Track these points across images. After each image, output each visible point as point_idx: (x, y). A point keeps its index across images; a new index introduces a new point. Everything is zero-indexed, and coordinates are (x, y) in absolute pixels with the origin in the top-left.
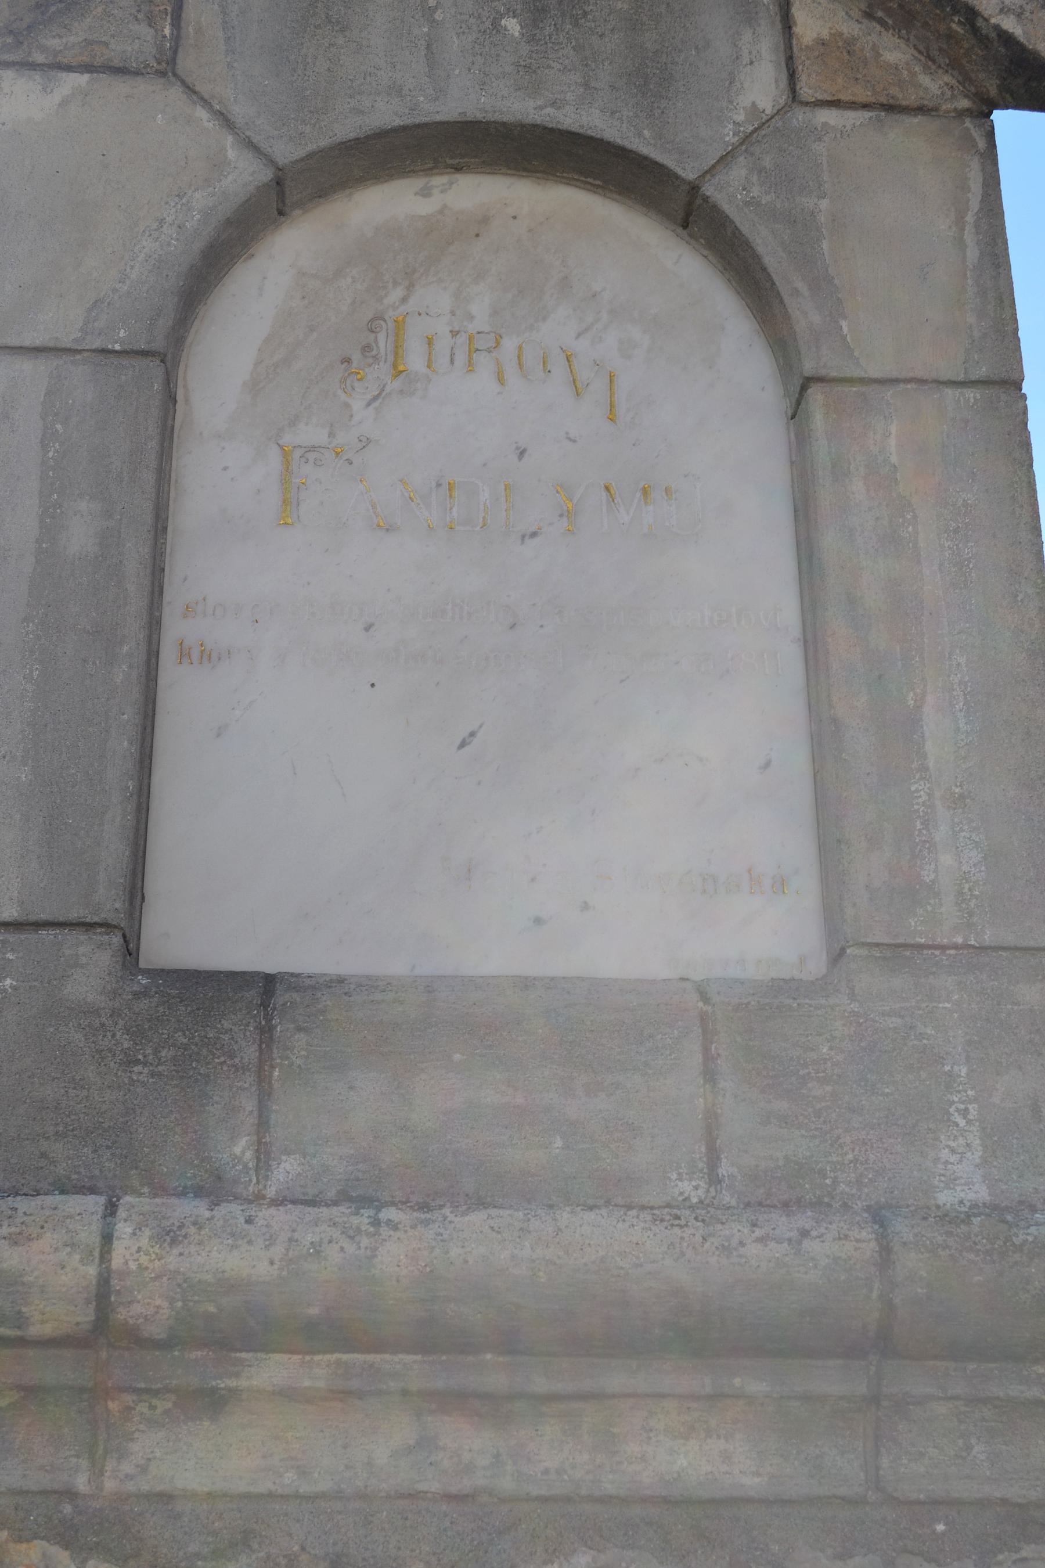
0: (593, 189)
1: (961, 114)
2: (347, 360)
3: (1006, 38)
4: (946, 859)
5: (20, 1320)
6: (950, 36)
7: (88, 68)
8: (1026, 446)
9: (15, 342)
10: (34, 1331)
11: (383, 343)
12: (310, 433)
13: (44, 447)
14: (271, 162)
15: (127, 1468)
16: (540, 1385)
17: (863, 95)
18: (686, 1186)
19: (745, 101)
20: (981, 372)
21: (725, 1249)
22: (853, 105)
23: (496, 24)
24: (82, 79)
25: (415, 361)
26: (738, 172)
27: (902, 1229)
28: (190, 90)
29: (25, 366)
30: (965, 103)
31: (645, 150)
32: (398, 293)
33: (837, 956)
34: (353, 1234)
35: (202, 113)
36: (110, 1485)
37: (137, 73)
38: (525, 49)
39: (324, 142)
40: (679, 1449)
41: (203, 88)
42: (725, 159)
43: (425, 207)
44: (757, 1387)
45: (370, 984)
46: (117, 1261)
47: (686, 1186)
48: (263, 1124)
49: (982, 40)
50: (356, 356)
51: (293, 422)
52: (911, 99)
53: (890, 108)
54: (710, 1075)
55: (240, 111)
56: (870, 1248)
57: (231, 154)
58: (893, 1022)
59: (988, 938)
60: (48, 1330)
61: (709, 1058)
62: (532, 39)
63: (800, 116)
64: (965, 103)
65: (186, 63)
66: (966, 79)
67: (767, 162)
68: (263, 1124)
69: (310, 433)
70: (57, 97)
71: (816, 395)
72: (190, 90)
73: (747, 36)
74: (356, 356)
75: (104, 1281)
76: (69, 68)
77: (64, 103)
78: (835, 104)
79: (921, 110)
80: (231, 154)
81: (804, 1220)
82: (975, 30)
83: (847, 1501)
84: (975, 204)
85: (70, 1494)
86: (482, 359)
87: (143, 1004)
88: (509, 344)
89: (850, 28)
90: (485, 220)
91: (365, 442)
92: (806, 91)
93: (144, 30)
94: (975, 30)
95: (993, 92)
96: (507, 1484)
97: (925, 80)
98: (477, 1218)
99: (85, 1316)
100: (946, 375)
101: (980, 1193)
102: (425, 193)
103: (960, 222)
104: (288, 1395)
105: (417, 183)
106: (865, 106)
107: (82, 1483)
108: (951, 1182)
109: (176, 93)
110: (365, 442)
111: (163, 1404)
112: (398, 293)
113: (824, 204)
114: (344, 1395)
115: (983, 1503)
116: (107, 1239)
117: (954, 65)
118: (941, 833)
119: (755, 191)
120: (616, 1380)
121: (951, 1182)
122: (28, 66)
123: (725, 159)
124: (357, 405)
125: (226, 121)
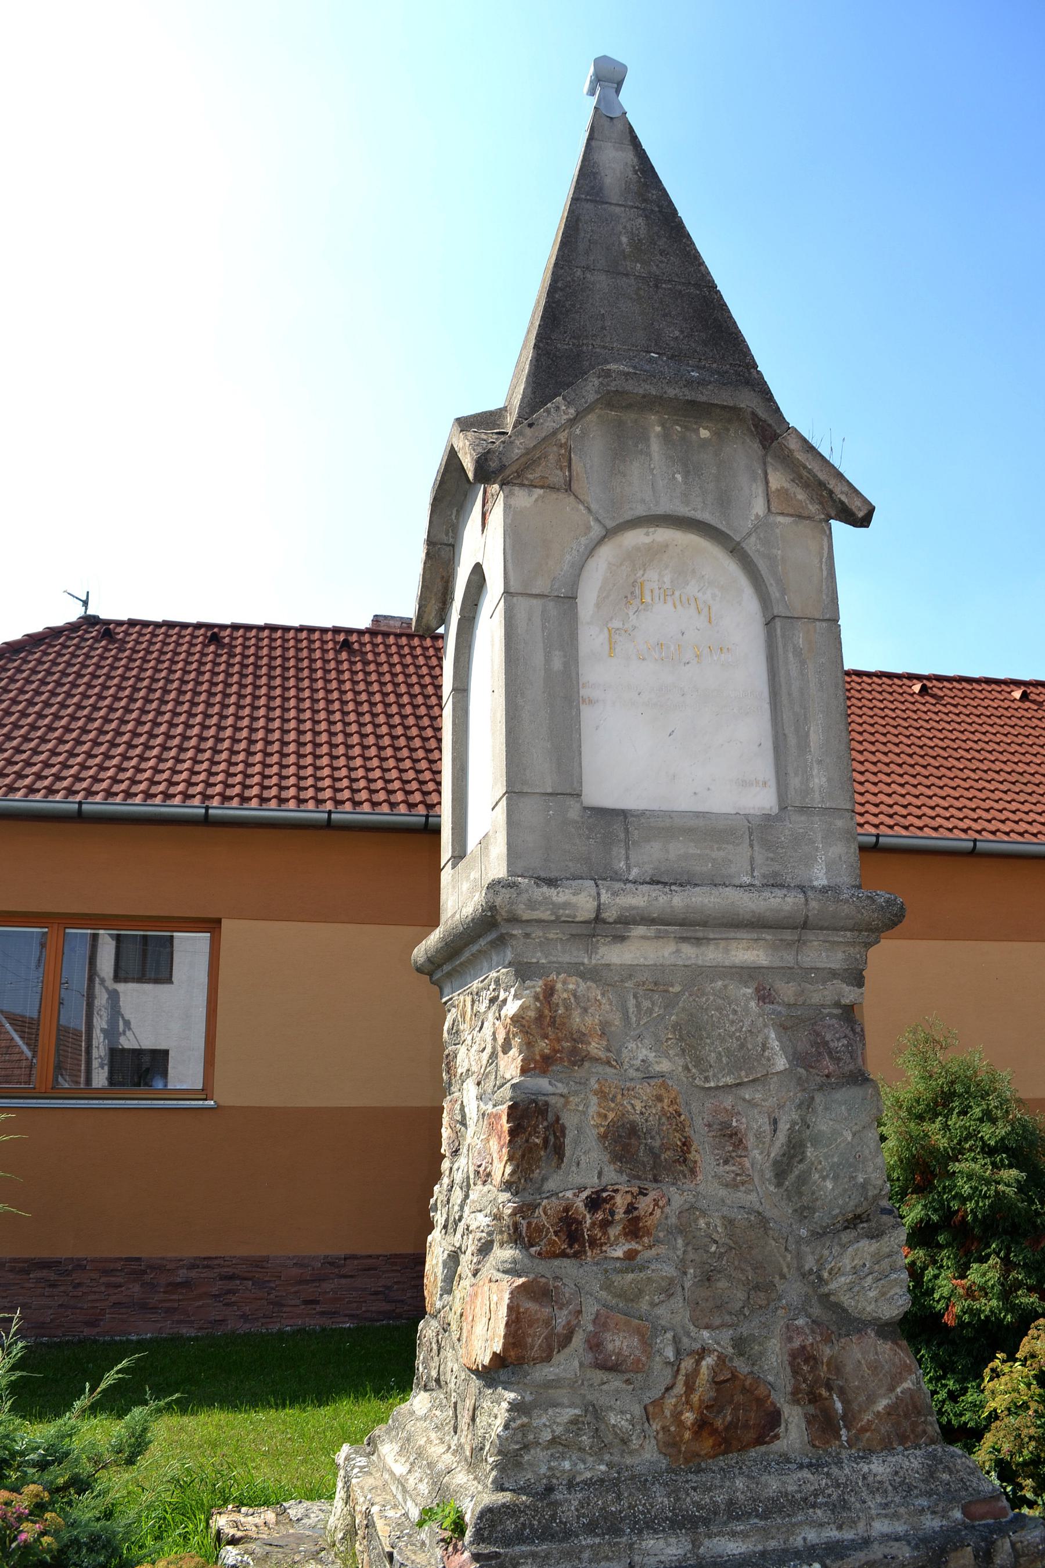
0: (701, 536)
1: (821, 521)
2: (626, 597)
3: (842, 503)
4: (816, 780)
5: (575, 916)
6: (821, 495)
7: (542, 487)
8: (840, 643)
9: (529, 592)
10: (577, 919)
11: (637, 592)
12: (616, 624)
13: (543, 632)
14: (604, 526)
15: (598, 957)
16: (711, 936)
17: (791, 511)
18: (745, 878)
19: (754, 512)
20: (827, 616)
21: (765, 900)
22: (788, 515)
23: (674, 477)
24: (540, 491)
25: (648, 598)
26: (753, 539)
27: (810, 893)
28: (576, 497)
29: (535, 602)
30: (823, 516)
31: (724, 529)
32: (641, 572)
33: (783, 808)
34: (666, 894)
35: (581, 507)
36: (594, 962)
37: (558, 490)
38: (683, 487)
39: (621, 521)
40: (678, 951)
41: (581, 497)
42: (749, 534)
43: (647, 540)
44: (769, 937)
45: (643, 813)
46: (602, 901)
47: (745, 878)
48: (627, 858)
49: (834, 501)
50: (629, 596)
51: (611, 619)
52: (806, 514)
53: (800, 517)
54: (751, 846)
55: (594, 507)
56: (803, 900)
57: (592, 523)
58: (801, 831)
59: (828, 806)
60: (581, 919)
61: (751, 840)
62: (685, 483)
63: (771, 518)
64: (823, 516)
65: (574, 486)
66: (824, 508)
67: (762, 536)
68: (627, 858)
69: (616, 624)
70: (535, 496)
71: (778, 623)
72: (576, 497)
73: (754, 486)
74: (629, 596)
75: (599, 906)
76: (536, 487)
77: (536, 500)
78: (782, 514)
79: (808, 518)
80: (592, 523)
81: (784, 891)
82: (831, 497)
83: (789, 968)
84: (825, 555)
85: (583, 964)
86: (669, 598)
87: (591, 820)
88: (677, 593)
89: (786, 485)
90: (667, 546)
91: (634, 628)
92: (773, 509)
93: (558, 472)
94: (831, 497)
95: (833, 515)
96: (700, 962)
97: (810, 507)
98: (697, 889)
99: (593, 916)
100: (817, 617)
101: (825, 882)
102: (647, 534)
103: (821, 562)
104: (644, 938)
105: (645, 530)
106: (792, 515)
107: (586, 961)
108: (817, 879)
109: (572, 498)
110: (634, 628)
111: (608, 939)
112: (641, 572)
113: (779, 552)
114: (657, 937)
115: (824, 969)
116: (599, 894)
117: (821, 503)
118: (815, 772)
119: (758, 547)
120: (732, 935)
121: (817, 879)
122: (522, 485)
123: (749, 534)
124: (631, 614)
125: (589, 509)
